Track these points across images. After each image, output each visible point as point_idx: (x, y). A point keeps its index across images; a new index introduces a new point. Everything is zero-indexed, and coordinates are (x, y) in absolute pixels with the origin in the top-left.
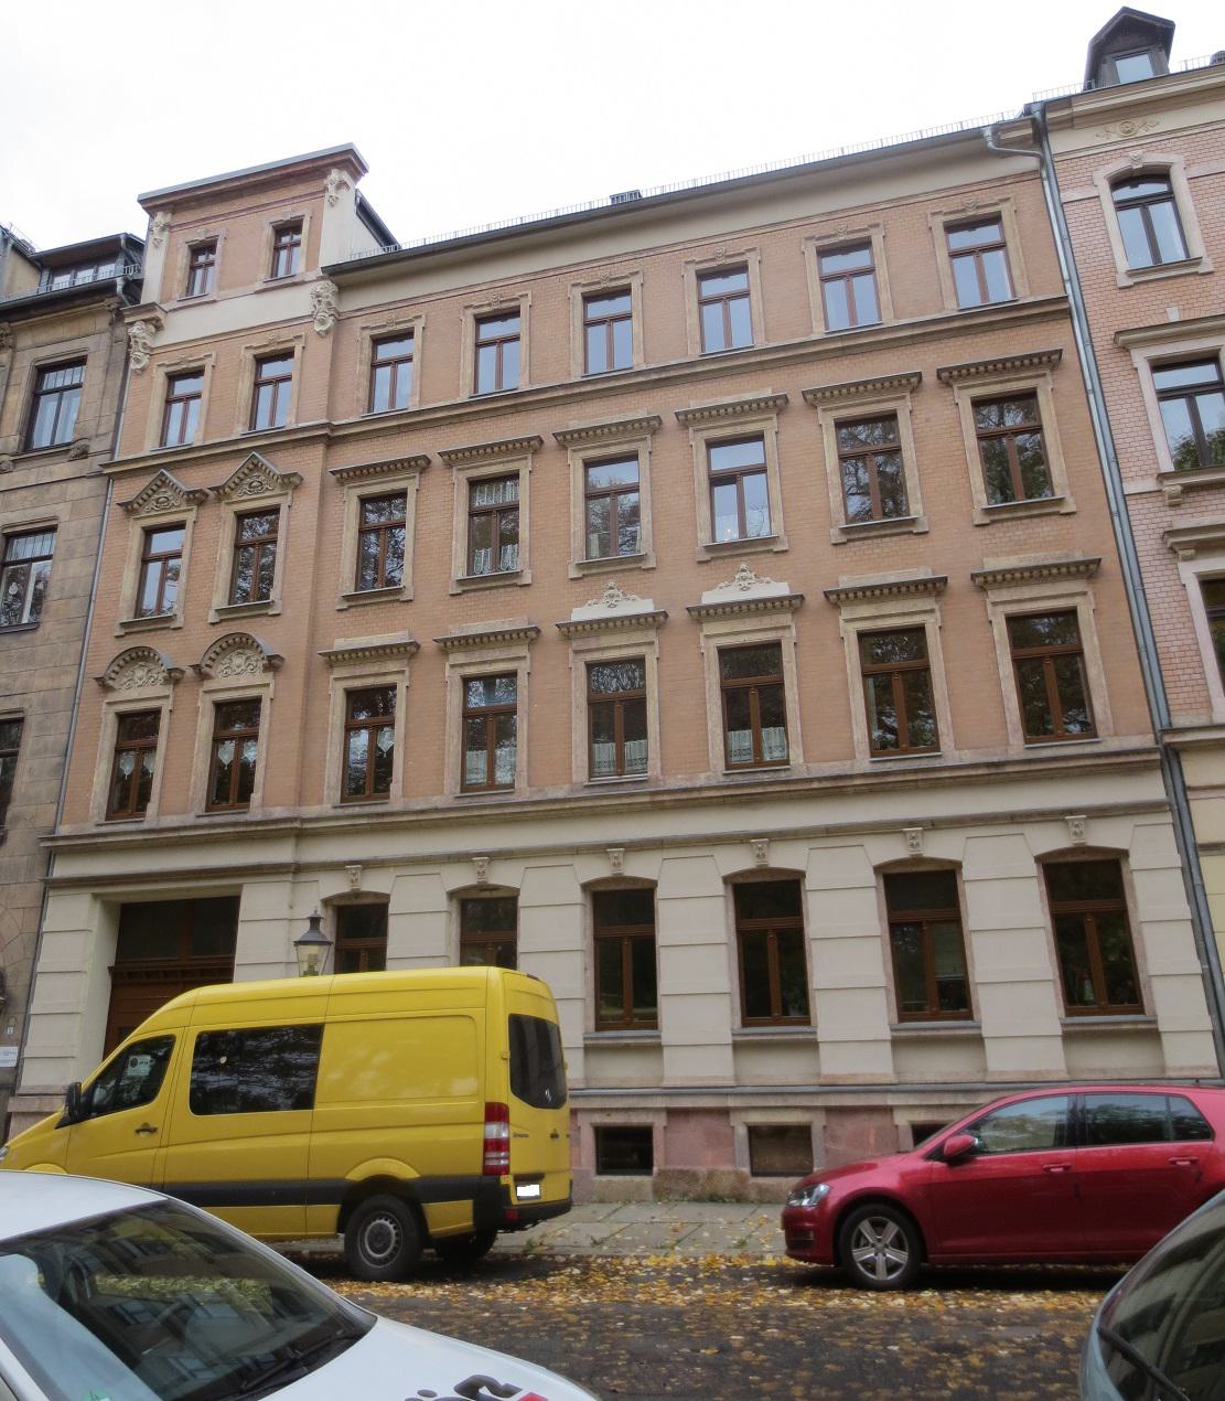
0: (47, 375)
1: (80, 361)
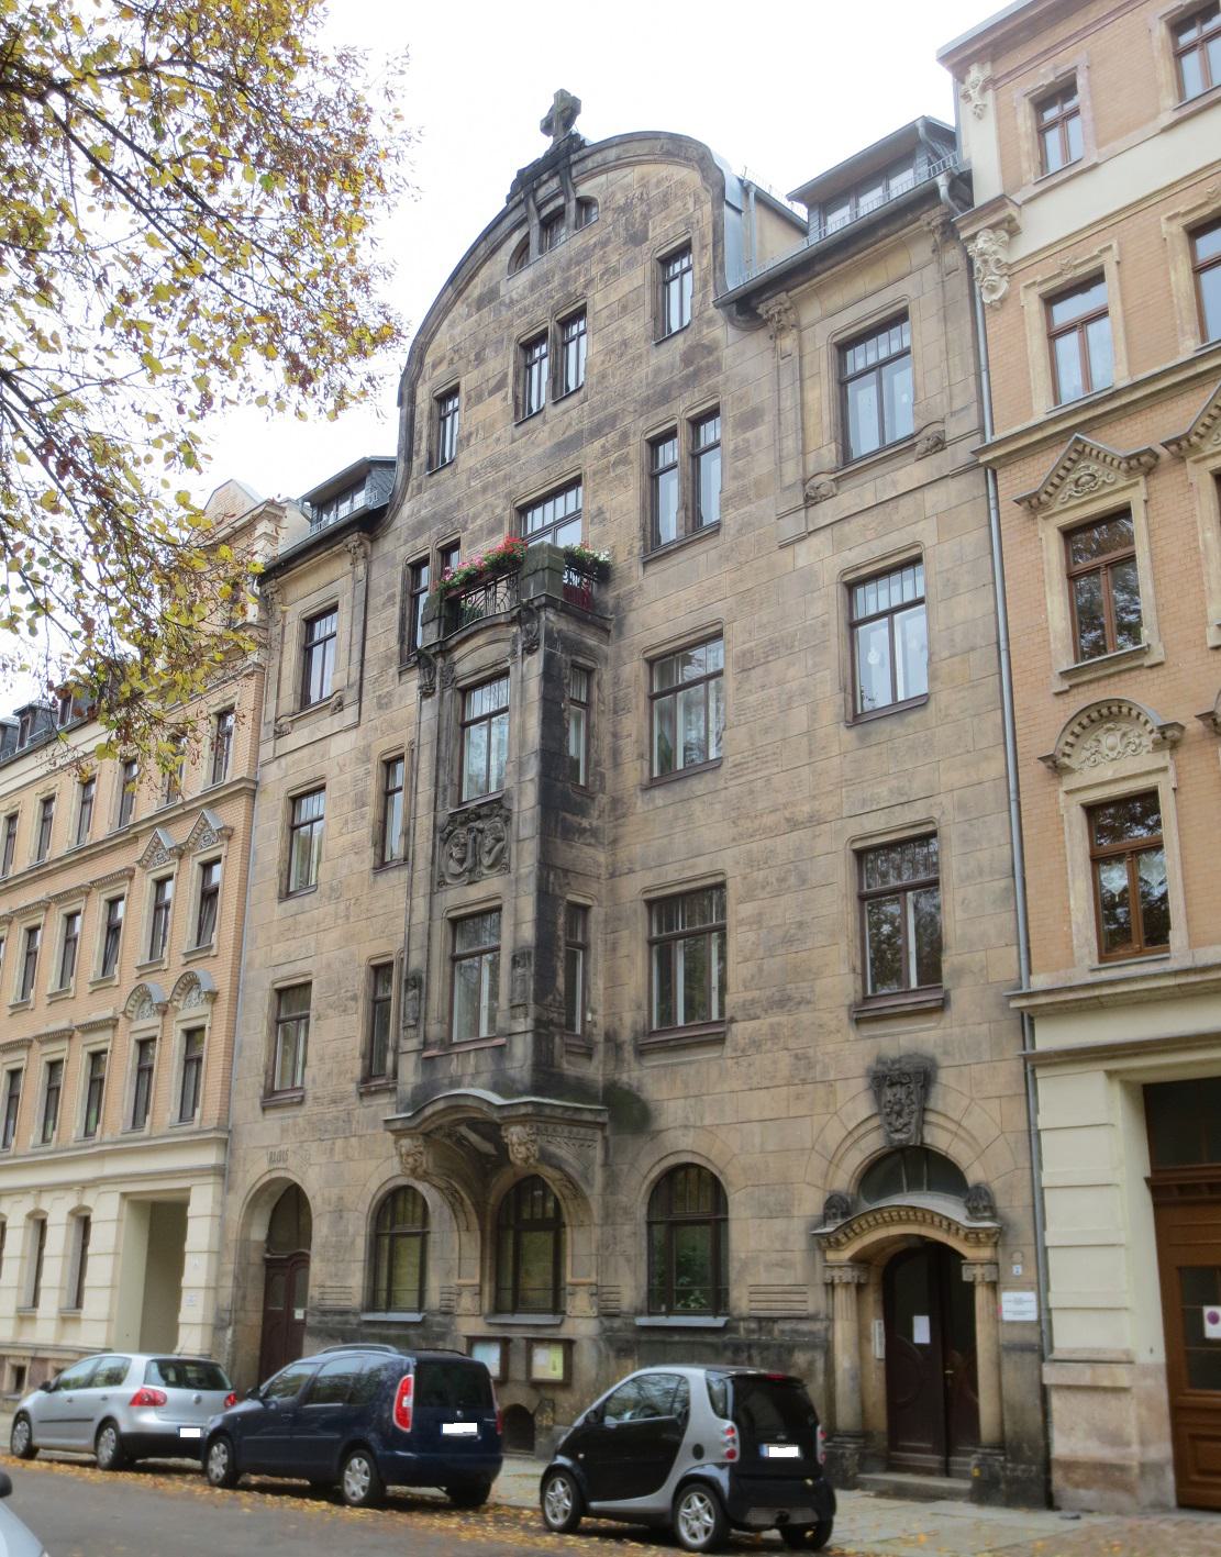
0: (661, 448)
1: (901, 317)
